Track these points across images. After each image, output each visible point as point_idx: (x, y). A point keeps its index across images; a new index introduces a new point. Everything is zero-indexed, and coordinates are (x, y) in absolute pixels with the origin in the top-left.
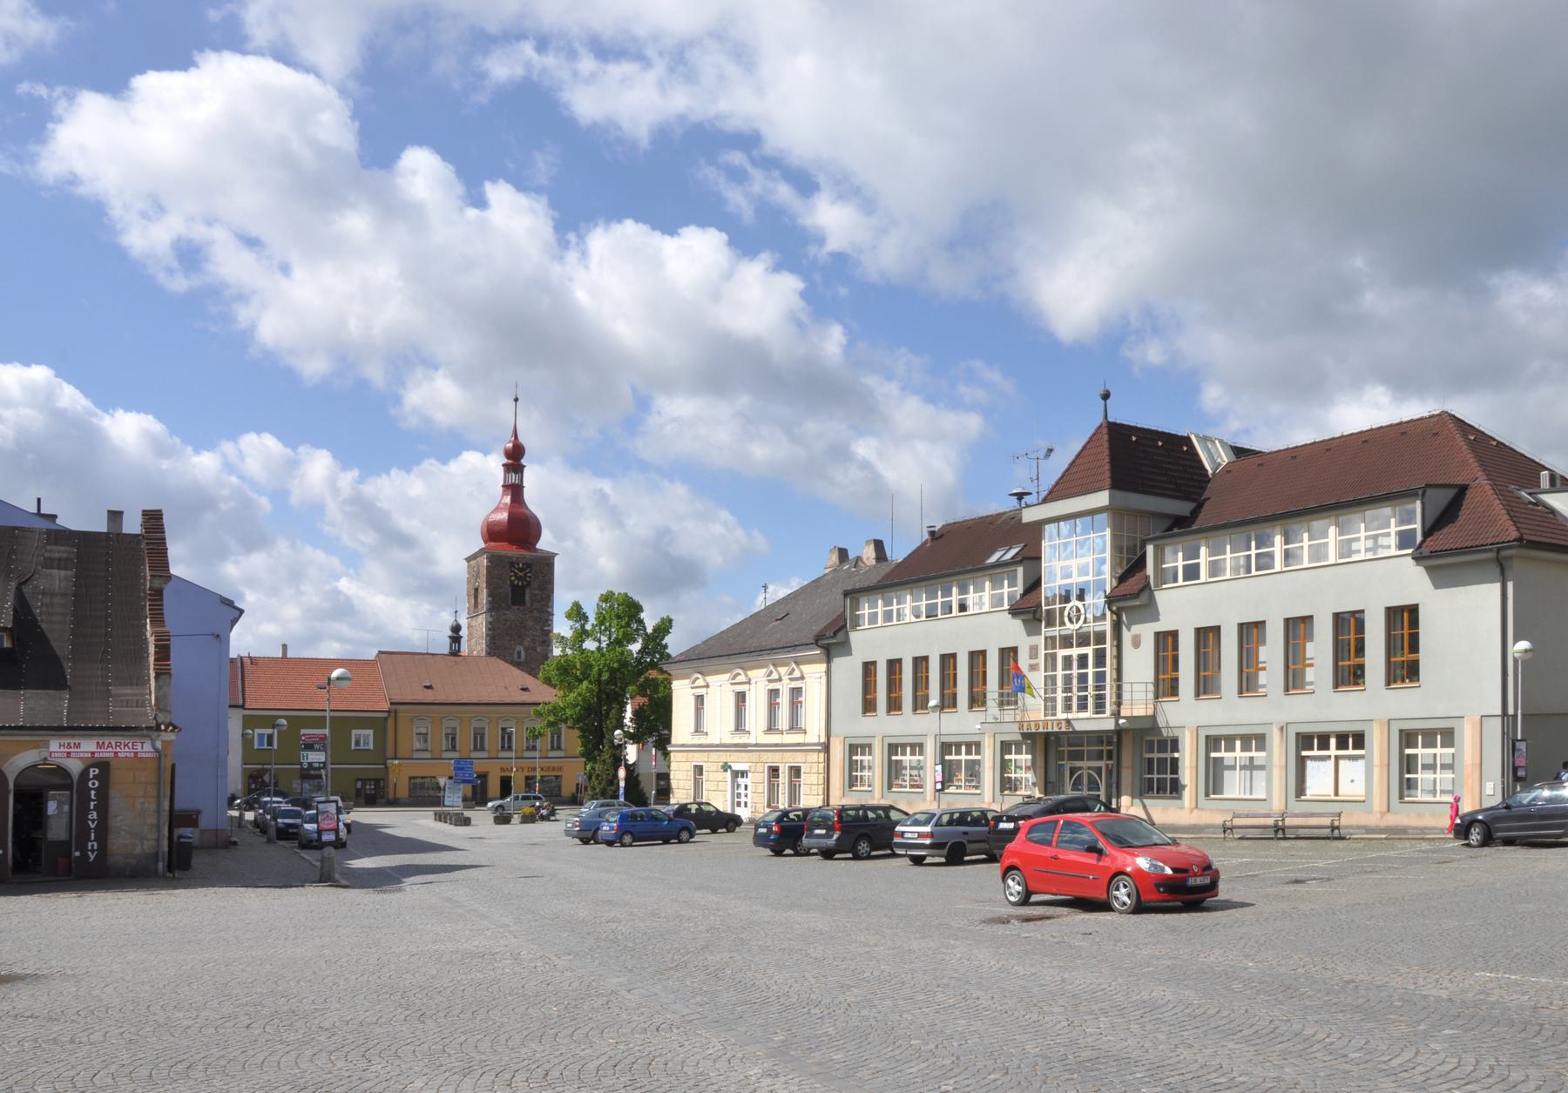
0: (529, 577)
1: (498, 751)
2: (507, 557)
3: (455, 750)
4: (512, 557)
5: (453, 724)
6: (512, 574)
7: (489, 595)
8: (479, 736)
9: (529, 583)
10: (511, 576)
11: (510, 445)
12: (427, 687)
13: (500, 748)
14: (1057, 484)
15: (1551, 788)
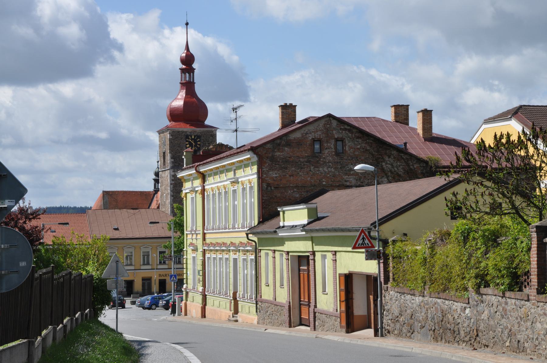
1: (157, 265)
2: (183, 132)
3: (166, 264)
4: (186, 132)
5: (130, 250)
6: (188, 143)
7: (172, 158)
8: (146, 256)
11: (184, 55)
12: (115, 229)
13: (158, 263)
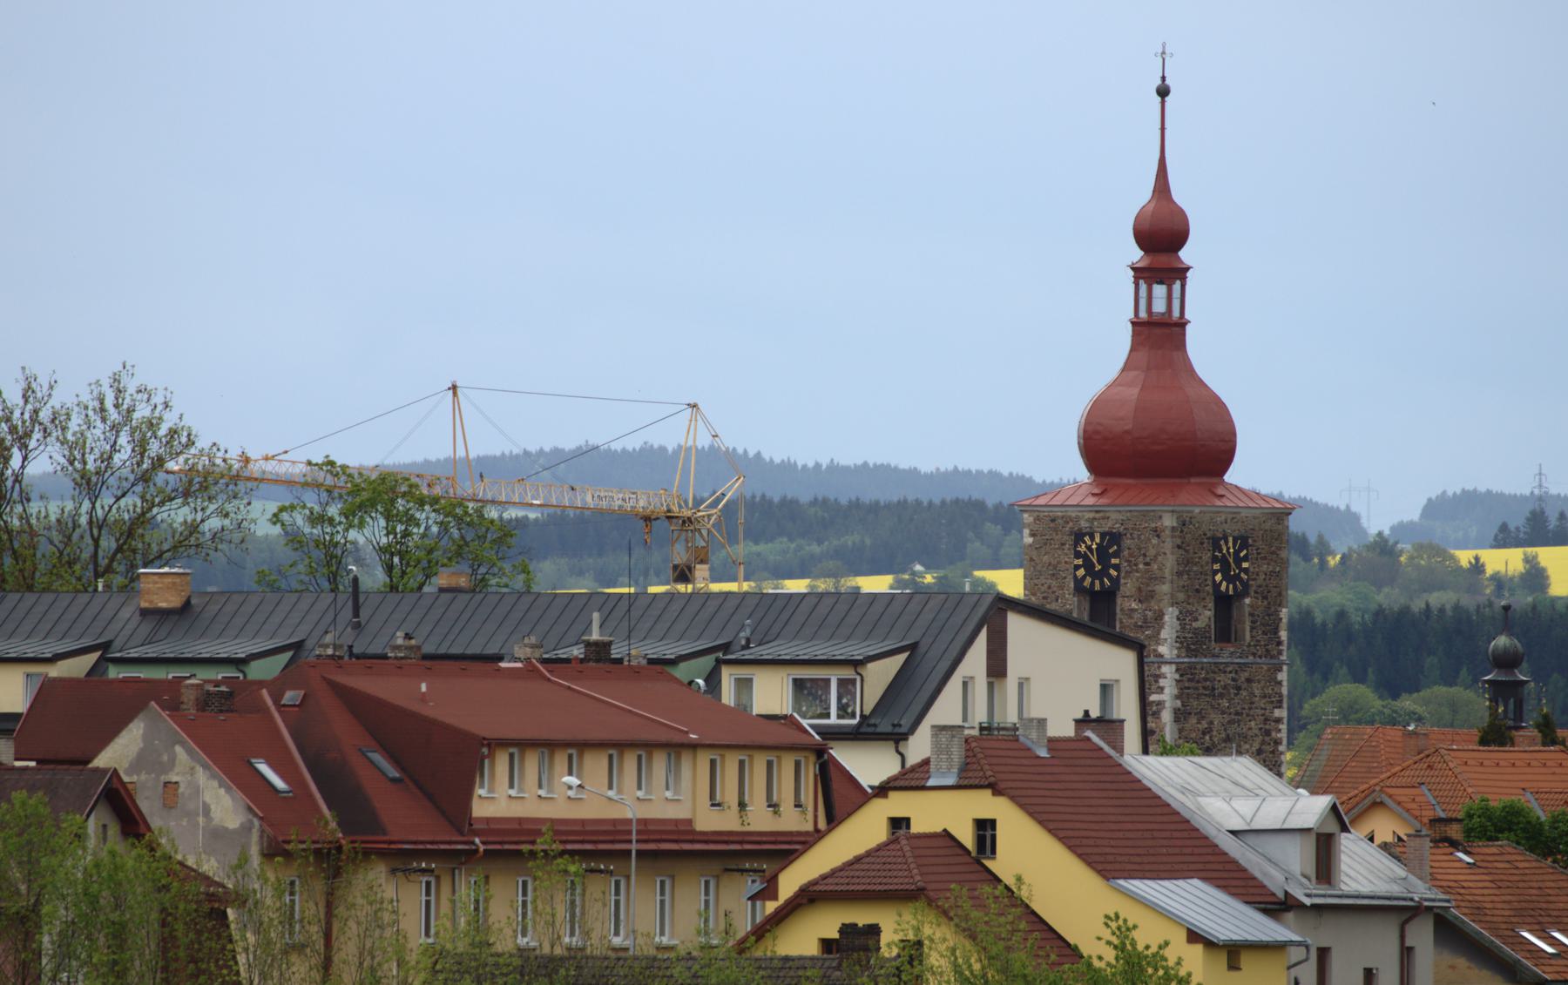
0: (1117, 567)
4: (1078, 519)
6: (1080, 562)
9: (1116, 582)
10: (1077, 567)
14: (868, 854)
15: (526, 517)
